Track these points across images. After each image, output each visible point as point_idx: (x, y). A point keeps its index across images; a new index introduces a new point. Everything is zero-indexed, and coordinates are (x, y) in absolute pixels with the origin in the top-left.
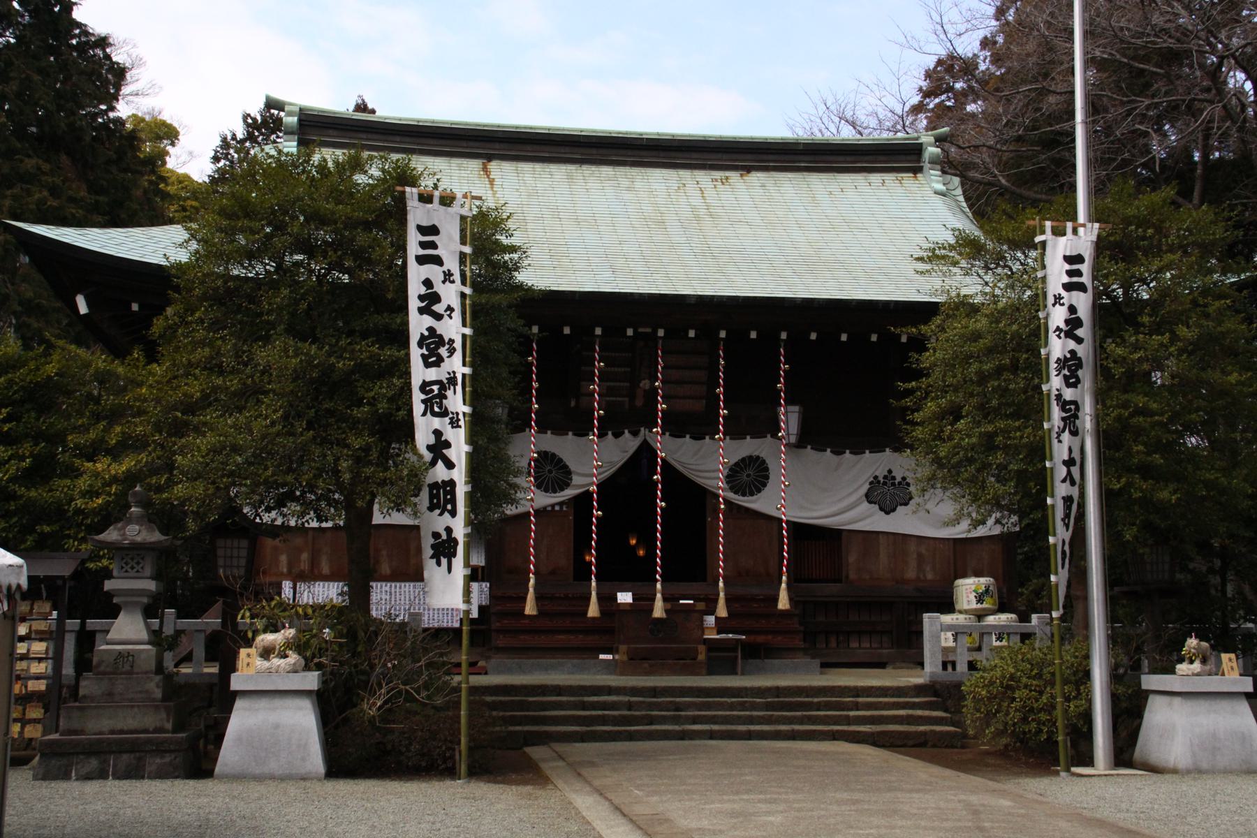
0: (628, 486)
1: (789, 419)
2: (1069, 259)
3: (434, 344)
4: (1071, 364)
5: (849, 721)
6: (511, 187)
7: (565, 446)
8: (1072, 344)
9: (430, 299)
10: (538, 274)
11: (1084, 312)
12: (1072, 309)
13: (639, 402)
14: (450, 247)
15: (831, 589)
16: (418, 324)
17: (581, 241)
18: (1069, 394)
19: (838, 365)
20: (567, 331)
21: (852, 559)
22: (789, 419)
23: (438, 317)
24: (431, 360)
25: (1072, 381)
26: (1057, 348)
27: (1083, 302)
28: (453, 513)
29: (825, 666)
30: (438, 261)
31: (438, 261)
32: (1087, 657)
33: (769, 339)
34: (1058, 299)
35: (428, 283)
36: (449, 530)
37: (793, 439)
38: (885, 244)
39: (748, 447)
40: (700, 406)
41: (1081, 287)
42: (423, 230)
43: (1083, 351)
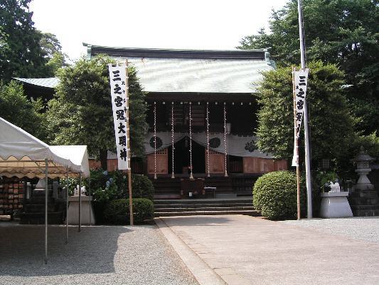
0: (181, 146)
1: (227, 127)
2: (301, 77)
3: (119, 101)
4: (300, 104)
5: (243, 209)
6: (137, 63)
7: (162, 136)
8: (301, 99)
9: (118, 89)
10: (148, 87)
11: (305, 90)
12: (301, 90)
13: (185, 123)
14: (124, 77)
15: (241, 174)
16: (114, 96)
17: (160, 79)
18: (299, 111)
19: (237, 111)
20: (164, 103)
21: (245, 166)
22: (227, 127)
23: (120, 93)
24: (119, 104)
25: (300, 107)
26: (297, 99)
27: (304, 88)
28: (125, 145)
29: (238, 196)
30: (120, 79)
31: (120, 79)
32: (305, 180)
33: (221, 105)
34: (297, 87)
35: (117, 85)
36: (124, 149)
37: (229, 133)
38: (245, 78)
39: (215, 136)
40: (203, 124)
41: (304, 84)
42: (114, 72)
43: (303, 100)
